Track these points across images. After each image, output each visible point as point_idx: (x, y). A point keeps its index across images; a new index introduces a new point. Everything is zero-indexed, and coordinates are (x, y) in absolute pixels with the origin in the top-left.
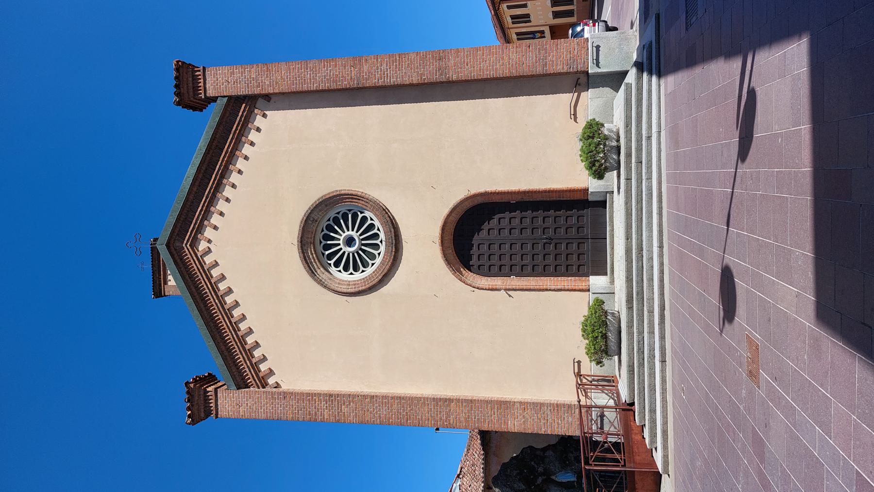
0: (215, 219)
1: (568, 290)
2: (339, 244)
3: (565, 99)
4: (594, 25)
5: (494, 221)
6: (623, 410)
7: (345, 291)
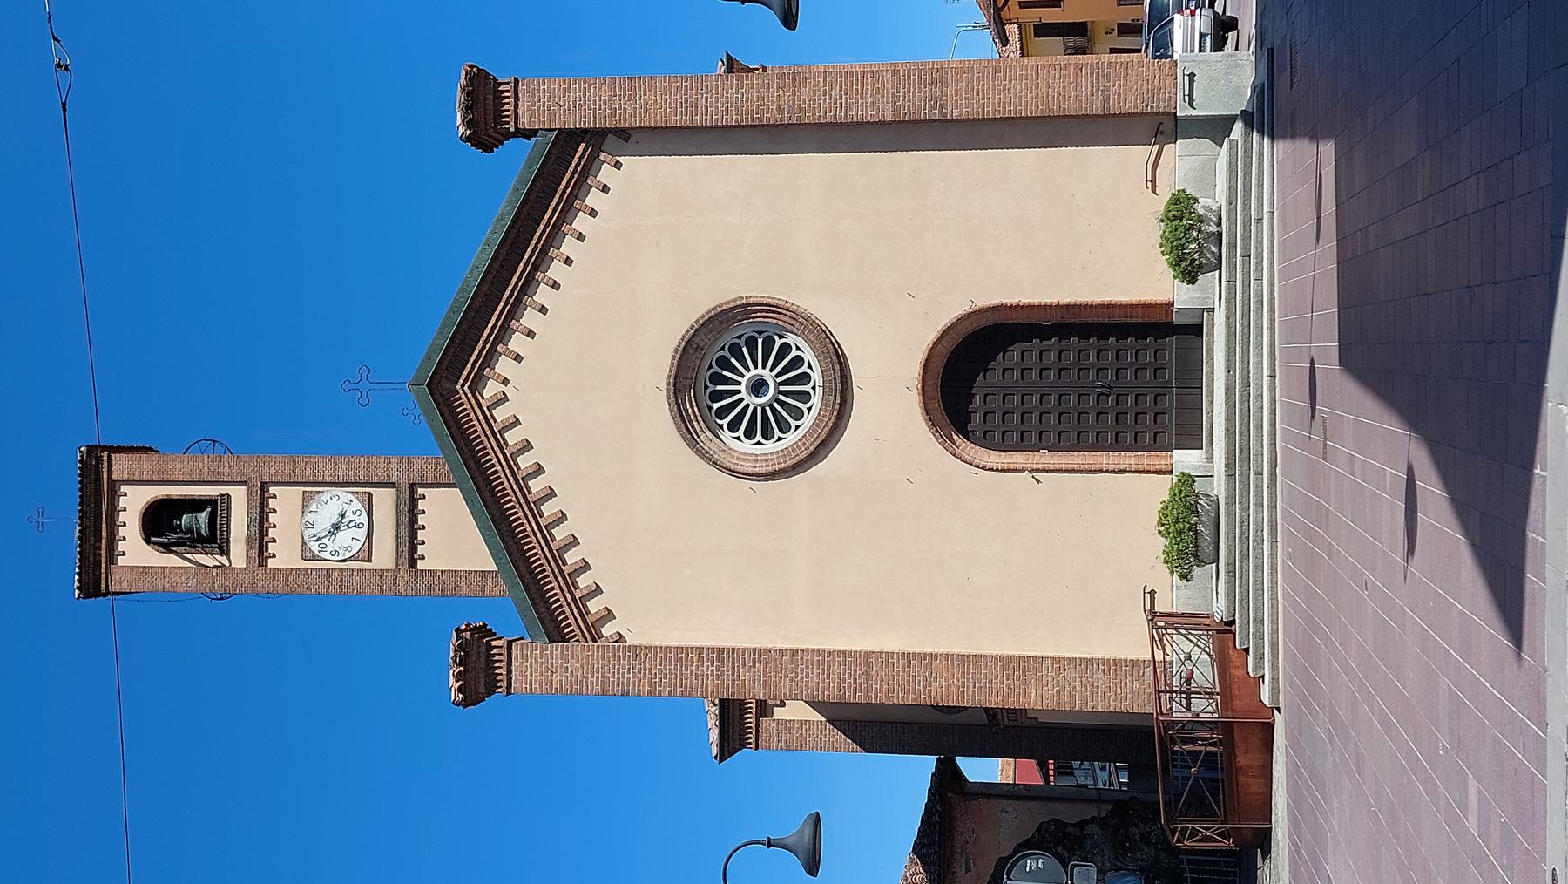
0: (517, 343)
1: (1137, 472)
2: (739, 392)
3: (1139, 154)
4: (1193, 13)
5: (1014, 353)
6: (1219, 631)
7: (750, 470)
